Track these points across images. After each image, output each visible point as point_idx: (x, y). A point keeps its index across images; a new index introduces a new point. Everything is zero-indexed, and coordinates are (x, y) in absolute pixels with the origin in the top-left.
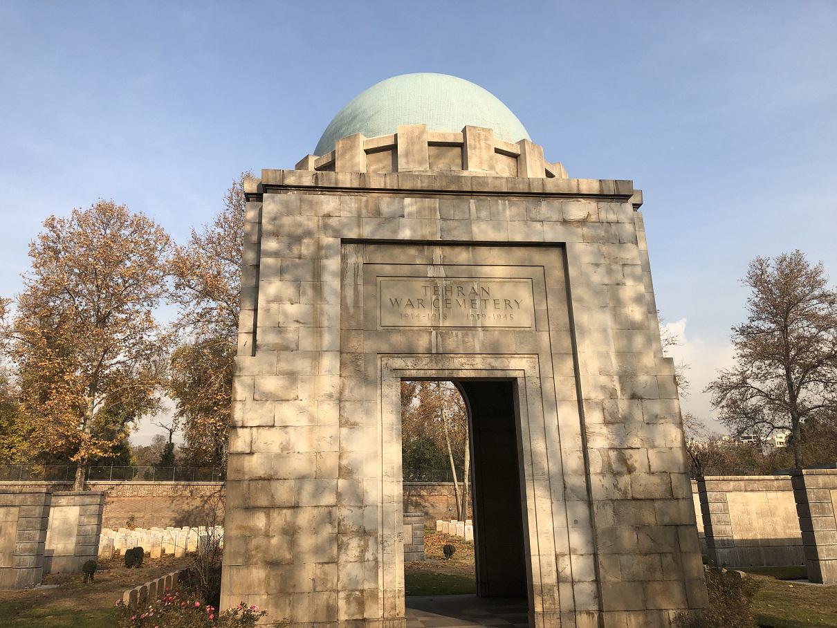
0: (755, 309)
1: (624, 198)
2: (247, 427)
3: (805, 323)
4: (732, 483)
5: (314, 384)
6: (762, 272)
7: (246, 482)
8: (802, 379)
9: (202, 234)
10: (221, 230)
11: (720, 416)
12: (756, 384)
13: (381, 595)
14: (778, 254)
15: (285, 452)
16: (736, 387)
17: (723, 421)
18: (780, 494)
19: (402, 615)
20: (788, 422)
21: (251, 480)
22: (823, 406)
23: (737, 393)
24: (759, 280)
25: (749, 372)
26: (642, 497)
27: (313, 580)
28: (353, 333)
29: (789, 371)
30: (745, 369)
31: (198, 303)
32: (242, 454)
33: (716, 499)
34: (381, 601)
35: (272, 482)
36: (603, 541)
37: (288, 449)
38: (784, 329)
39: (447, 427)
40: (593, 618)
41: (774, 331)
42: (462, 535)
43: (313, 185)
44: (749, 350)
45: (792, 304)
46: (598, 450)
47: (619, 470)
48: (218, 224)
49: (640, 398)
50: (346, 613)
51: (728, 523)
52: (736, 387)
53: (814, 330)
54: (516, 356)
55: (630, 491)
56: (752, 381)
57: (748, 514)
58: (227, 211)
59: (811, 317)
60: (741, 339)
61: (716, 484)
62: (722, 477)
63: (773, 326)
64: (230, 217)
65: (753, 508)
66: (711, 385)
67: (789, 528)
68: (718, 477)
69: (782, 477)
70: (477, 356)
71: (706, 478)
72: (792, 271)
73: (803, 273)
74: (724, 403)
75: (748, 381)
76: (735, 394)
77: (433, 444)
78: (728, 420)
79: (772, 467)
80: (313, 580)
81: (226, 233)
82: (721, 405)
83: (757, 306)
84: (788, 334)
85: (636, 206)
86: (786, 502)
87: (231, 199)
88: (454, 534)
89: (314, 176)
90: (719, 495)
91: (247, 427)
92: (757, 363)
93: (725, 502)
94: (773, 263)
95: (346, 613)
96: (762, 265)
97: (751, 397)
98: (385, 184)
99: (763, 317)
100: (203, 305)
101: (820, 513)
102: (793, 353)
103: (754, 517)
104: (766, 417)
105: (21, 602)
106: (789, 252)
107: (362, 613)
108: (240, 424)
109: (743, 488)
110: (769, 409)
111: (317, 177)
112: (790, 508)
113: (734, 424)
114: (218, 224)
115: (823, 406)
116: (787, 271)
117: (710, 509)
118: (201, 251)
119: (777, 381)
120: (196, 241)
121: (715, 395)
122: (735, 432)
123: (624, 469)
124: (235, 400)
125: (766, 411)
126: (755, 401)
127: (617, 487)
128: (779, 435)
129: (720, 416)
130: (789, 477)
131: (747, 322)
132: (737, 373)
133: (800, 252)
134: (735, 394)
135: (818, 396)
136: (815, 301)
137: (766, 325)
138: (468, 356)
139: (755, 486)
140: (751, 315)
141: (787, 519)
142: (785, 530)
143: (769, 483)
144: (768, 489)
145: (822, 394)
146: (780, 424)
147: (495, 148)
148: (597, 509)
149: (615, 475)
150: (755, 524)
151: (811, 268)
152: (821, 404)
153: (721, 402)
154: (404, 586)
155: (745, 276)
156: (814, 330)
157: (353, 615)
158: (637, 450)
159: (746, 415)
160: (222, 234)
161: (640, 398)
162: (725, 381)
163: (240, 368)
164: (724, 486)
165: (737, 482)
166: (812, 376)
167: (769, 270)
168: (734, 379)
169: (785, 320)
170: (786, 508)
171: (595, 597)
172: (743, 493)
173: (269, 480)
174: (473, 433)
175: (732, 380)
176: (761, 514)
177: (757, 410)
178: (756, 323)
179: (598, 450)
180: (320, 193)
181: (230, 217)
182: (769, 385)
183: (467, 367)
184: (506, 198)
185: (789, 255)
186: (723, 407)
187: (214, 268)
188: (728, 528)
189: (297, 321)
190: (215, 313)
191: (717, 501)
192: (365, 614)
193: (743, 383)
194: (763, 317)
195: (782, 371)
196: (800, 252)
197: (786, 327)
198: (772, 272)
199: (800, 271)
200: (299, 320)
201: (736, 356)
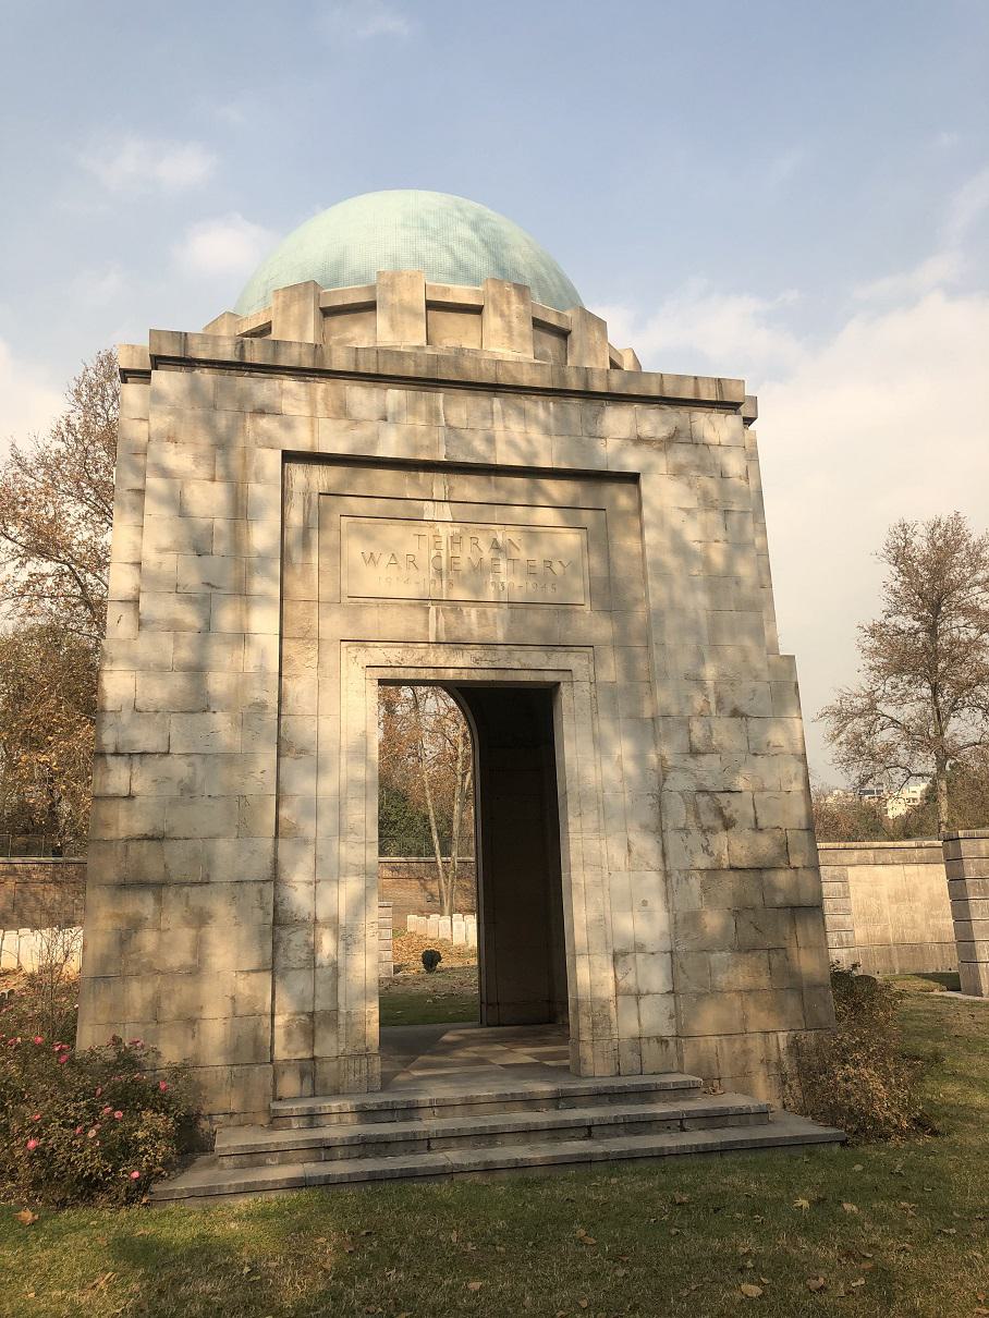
0: (892, 598)
1: (732, 407)
2: (122, 755)
3: (962, 621)
4: (856, 853)
5: (596, 356)
6: (906, 542)
7: (121, 843)
8: (954, 704)
9: (29, 452)
10: (62, 446)
11: (835, 757)
12: (890, 711)
13: (341, 1021)
14: (930, 517)
15: (187, 796)
16: (861, 714)
17: (839, 765)
18: (922, 868)
19: (375, 1050)
20: (931, 768)
21: (129, 840)
22: (980, 743)
23: (862, 724)
24: (900, 556)
25: (880, 692)
26: (745, 865)
27: (233, 998)
28: (301, 607)
29: (935, 689)
30: (875, 688)
31: (22, 564)
32: (115, 797)
33: (834, 877)
34: (342, 1030)
35: (165, 844)
36: (686, 932)
37: (191, 791)
38: (932, 630)
39: (429, 771)
40: (667, 1047)
41: (917, 632)
42: (448, 937)
43: (236, 359)
44: (882, 660)
45: (948, 591)
46: (681, 794)
47: (711, 824)
48: (59, 435)
49: (743, 715)
50: (284, 1049)
51: (848, 912)
52: (861, 714)
53: (973, 633)
54: (559, 648)
55: (725, 857)
56: (883, 704)
57: (878, 898)
58: (71, 415)
59: (971, 611)
60: (871, 643)
61: (835, 855)
62: (842, 845)
63: (917, 624)
64: (77, 423)
65: (885, 889)
66: (824, 711)
67: (933, 917)
68: (836, 845)
69: (926, 843)
70: (499, 647)
71: (821, 845)
72: (947, 544)
73: (963, 547)
74: (842, 737)
75: (878, 705)
76: (858, 725)
77: (405, 800)
78: (847, 762)
79: (909, 828)
80: (233, 998)
81: (70, 450)
82: (838, 741)
83: (895, 593)
84: (937, 637)
85: (748, 421)
86: (933, 880)
87: (78, 393)
88: (435, 936)
89: (239, 346)
90: (837, 871)
91: (122, 755)
92: (893, 679)
93: (845, 881)
94: (922, 530)
95: (284, 1049)
96: (906, 533)
97: (882, 729)
98: (356, 365)
99: (904, 610)
100: (31, 567)
101: (980, 894)
102: (942, 665)
103: (885, 902)
104: (901, 759)
105: (494, 231)
106: (945, 515)
107: (312, 1047)
108: (111, 749)
109: (871, 861)
110: (906, 748)
111: (242, 347)
112: (935, 888)
113: (855, 770)
114: (59, 435)
115: (980, 743)
116: (940, 543)
117: (824, 891)
118: (27, 478)
119: (920, 705)
120: (19, 461)
121: (830, 725)
122: (856, 782)
123: (718, 823)
124: (103, 710)
125: (901, 750)
126: (887, 735)
127: (707, 850)
128: (912, 789)
129: (835, 757)
130: (940, 843)
131: (880, 618)
132: (863, 693)
133: (960, 515)
134: (858, 725)
135: (974, 728)
136: (977, 589)
137: (906, 623)
138: (485, 647)
139: (889, 856)
140: (887, 607)
141: (934, 904)
142: (927, 920)
143: (909, 852)
144: (907, 862)
145: (980, 726)
146: (919, 771)
147: (533, 318)
148: (678, 883)
149: (704, 832)
150: (887, 913)
151: (974, 539)
152: (977, 740)
153: (838, 735)
154: (377, 1005)
155: (881, 548)
156: (973, 633)
157: (296, 1053)
158: (737, 795)
159: (873, 756)
160: (63, 450)
161: (743, 715)
162: (846, 705)
163: (111, 658)
164: (846, 857)
165: (863, 851)
166: (967, 699)
167: (916, 540)
168: (859, 703)
169: (936, 617)
170: (930, 889)
171: (671, 1017)
172: (870, 867)
173: (158, 839)
174: (481, 775)
175: (855, 704)
176: (896, 898)
177: (889, 749)
178: (892, 620)
179: (681, 794)
180: (247, 373)
181: (77, 423)
182: (909, 712)
183: (484, 665)
184: (550, 398)
185: (945, 519)
186: (841, 743)
187: (50, 507)
188: (848, 919)
189: (208, 584)
190: (50, 582)
191: (834, 879)
192: (315, 1049)
193: (872, 707)
194: (904, 610)
195: (926, 692)
196: (960, 515)
197: (935, 625)
198: (920, 543)
199: (958, 543)
200: (212, 582)
201: (862, 668)
